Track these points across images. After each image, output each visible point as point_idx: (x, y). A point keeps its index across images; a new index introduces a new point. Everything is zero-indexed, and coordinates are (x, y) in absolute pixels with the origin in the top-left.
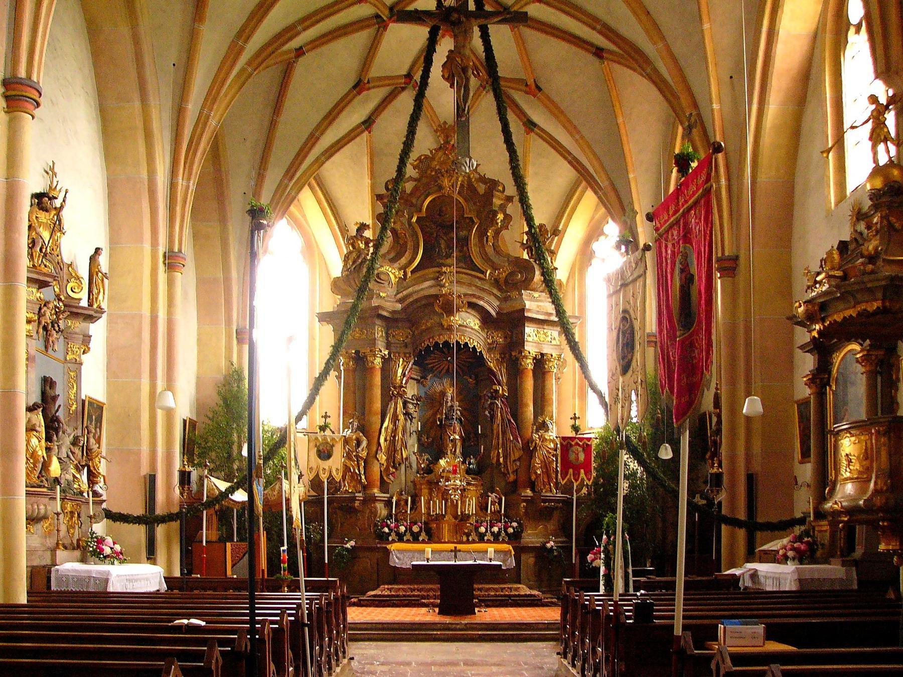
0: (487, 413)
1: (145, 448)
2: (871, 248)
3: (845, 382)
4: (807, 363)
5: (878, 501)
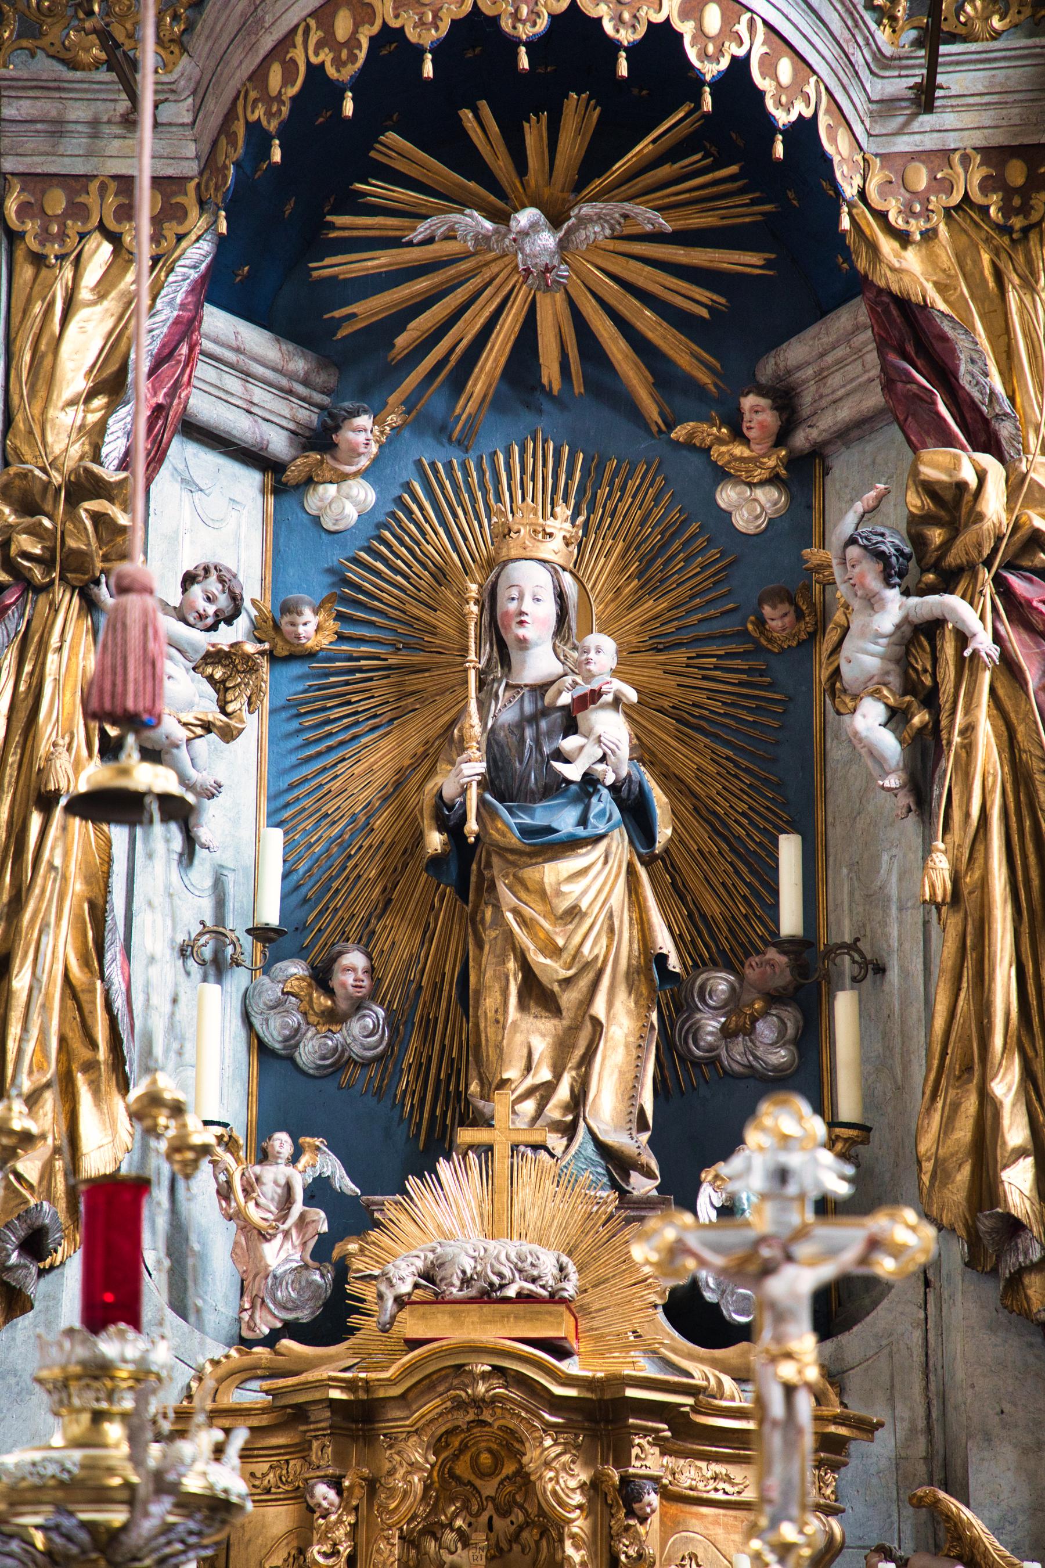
0: (869, 720)
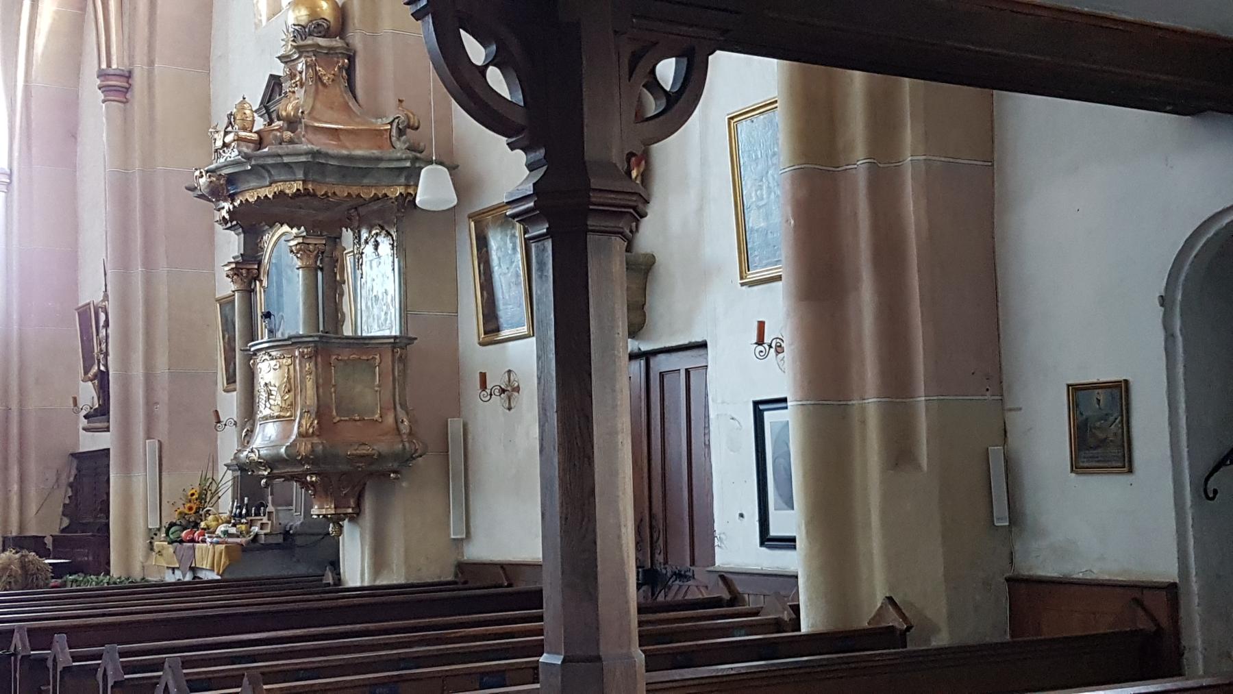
2: (290, 108)
3: (279, 275)
4: (231, 244)
5: (304, 448)
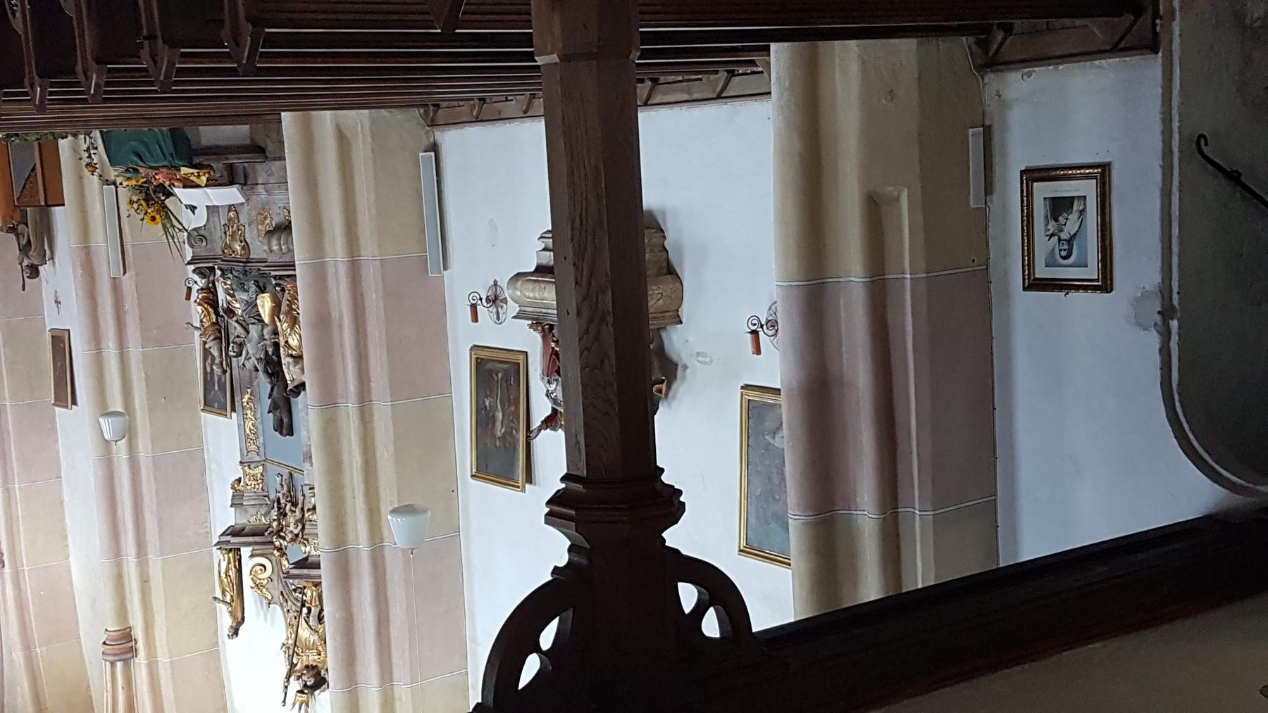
1: (135, 351)
